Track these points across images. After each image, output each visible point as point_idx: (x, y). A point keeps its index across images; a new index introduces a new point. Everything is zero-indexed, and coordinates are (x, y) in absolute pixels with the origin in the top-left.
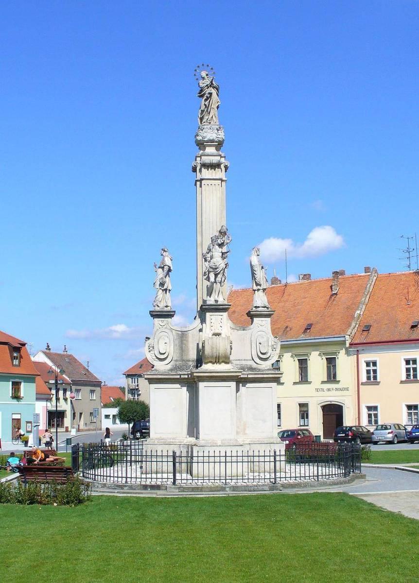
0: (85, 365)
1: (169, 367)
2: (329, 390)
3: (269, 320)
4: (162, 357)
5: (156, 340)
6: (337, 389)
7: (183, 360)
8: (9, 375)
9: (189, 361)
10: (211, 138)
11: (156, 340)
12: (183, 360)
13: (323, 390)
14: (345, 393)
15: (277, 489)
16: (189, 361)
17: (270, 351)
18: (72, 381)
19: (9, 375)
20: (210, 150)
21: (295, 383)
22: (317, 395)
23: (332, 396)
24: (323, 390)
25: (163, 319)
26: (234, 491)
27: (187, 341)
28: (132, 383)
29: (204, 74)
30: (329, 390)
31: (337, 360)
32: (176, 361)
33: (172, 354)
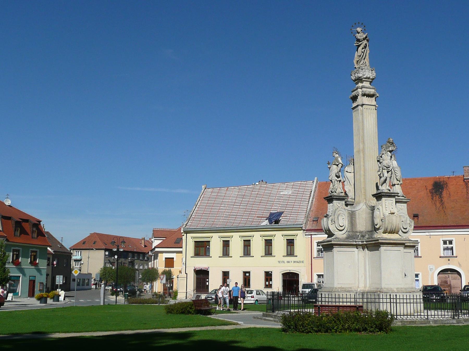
0: (59, 240)
1: (345, 236)
2: (288, 262)
3: (405, 205)
4: (341, 228)
5: (336, 216)
6: (295, 262)
7: (353, 232)
8: (31, 245)
9: (357, 232)
10: (368, 76)
11: (336, 216)
12: (353, 232)
13: (284, 262)
14: (301, 264)
15: (461, 323)
16: (357, 232)
17: (408, 227)
18: (54, 252)
19: (31, 245)
20: (367, 84)
21: (262, 257)
22: (279, 265)
23: (291, 266)
24: (284, 262)
25: (339, 202)
26: (435, 323)
27: (355, 218)
28: (181, 252)
29: (359, 29)
30: (288, 262)
31: (211, 243)
32: (349, 232)
33: (347, 226)
